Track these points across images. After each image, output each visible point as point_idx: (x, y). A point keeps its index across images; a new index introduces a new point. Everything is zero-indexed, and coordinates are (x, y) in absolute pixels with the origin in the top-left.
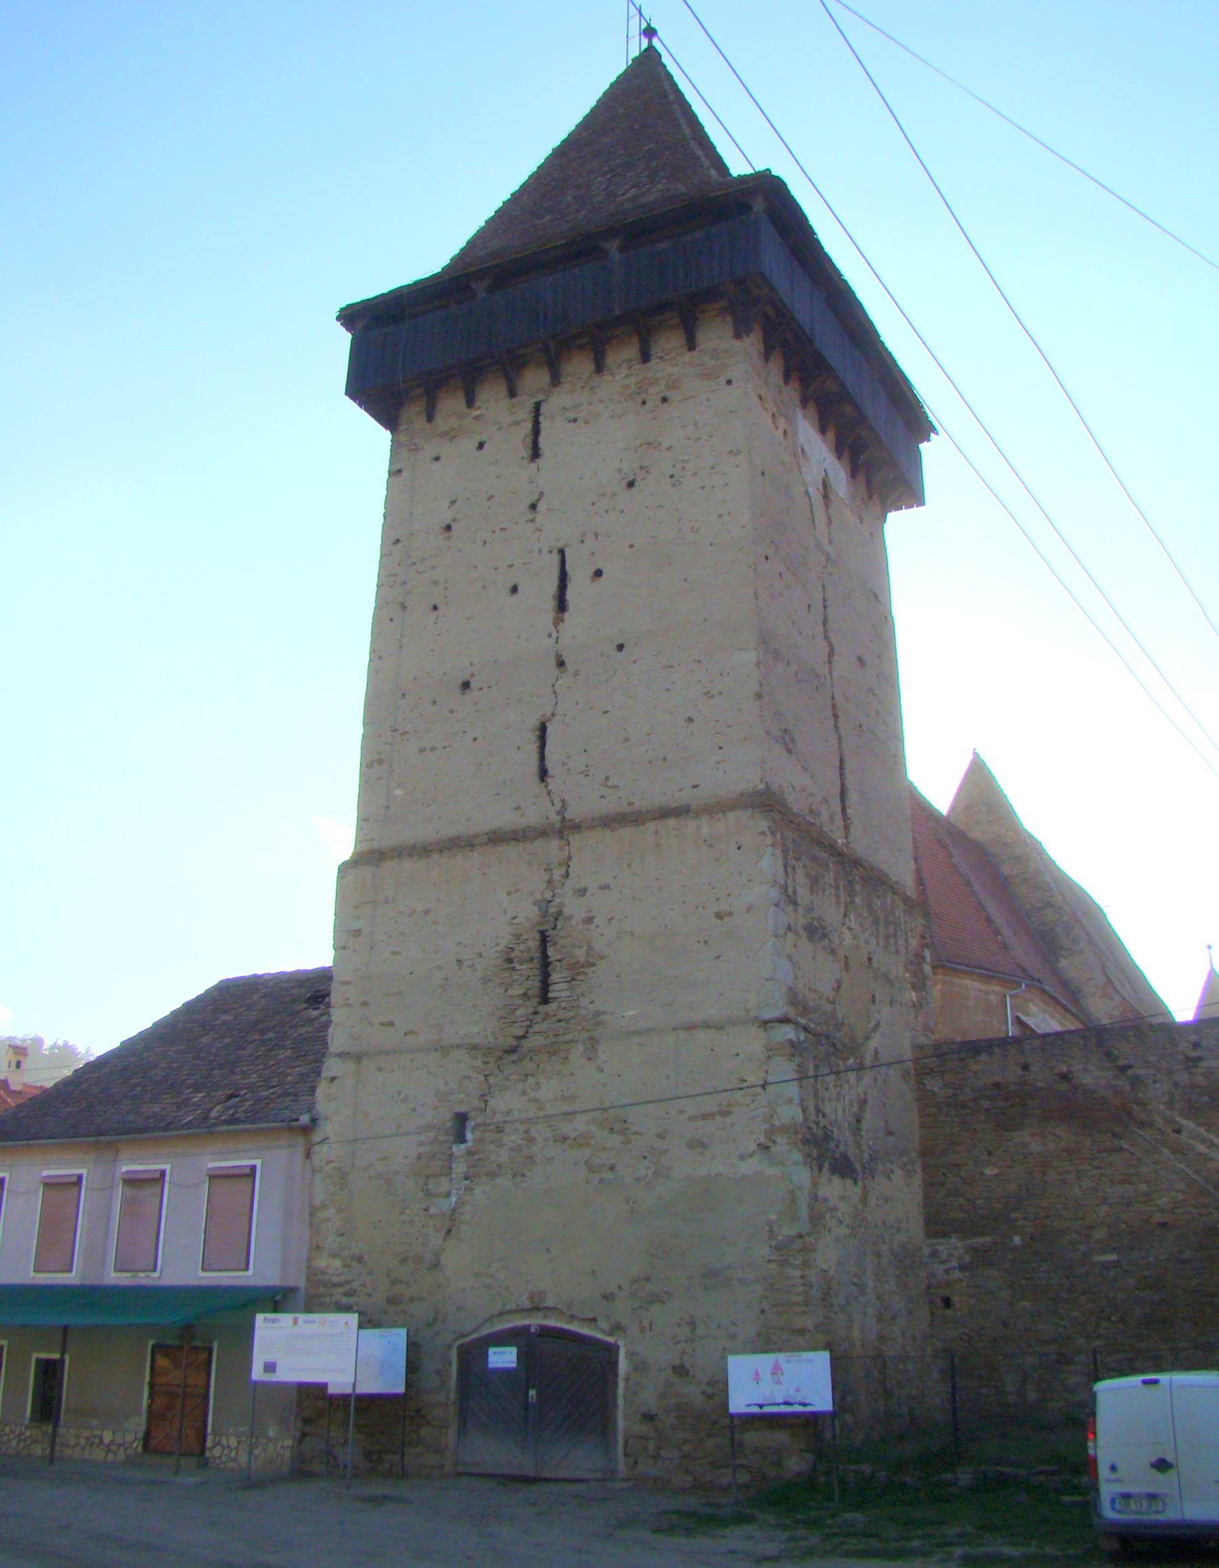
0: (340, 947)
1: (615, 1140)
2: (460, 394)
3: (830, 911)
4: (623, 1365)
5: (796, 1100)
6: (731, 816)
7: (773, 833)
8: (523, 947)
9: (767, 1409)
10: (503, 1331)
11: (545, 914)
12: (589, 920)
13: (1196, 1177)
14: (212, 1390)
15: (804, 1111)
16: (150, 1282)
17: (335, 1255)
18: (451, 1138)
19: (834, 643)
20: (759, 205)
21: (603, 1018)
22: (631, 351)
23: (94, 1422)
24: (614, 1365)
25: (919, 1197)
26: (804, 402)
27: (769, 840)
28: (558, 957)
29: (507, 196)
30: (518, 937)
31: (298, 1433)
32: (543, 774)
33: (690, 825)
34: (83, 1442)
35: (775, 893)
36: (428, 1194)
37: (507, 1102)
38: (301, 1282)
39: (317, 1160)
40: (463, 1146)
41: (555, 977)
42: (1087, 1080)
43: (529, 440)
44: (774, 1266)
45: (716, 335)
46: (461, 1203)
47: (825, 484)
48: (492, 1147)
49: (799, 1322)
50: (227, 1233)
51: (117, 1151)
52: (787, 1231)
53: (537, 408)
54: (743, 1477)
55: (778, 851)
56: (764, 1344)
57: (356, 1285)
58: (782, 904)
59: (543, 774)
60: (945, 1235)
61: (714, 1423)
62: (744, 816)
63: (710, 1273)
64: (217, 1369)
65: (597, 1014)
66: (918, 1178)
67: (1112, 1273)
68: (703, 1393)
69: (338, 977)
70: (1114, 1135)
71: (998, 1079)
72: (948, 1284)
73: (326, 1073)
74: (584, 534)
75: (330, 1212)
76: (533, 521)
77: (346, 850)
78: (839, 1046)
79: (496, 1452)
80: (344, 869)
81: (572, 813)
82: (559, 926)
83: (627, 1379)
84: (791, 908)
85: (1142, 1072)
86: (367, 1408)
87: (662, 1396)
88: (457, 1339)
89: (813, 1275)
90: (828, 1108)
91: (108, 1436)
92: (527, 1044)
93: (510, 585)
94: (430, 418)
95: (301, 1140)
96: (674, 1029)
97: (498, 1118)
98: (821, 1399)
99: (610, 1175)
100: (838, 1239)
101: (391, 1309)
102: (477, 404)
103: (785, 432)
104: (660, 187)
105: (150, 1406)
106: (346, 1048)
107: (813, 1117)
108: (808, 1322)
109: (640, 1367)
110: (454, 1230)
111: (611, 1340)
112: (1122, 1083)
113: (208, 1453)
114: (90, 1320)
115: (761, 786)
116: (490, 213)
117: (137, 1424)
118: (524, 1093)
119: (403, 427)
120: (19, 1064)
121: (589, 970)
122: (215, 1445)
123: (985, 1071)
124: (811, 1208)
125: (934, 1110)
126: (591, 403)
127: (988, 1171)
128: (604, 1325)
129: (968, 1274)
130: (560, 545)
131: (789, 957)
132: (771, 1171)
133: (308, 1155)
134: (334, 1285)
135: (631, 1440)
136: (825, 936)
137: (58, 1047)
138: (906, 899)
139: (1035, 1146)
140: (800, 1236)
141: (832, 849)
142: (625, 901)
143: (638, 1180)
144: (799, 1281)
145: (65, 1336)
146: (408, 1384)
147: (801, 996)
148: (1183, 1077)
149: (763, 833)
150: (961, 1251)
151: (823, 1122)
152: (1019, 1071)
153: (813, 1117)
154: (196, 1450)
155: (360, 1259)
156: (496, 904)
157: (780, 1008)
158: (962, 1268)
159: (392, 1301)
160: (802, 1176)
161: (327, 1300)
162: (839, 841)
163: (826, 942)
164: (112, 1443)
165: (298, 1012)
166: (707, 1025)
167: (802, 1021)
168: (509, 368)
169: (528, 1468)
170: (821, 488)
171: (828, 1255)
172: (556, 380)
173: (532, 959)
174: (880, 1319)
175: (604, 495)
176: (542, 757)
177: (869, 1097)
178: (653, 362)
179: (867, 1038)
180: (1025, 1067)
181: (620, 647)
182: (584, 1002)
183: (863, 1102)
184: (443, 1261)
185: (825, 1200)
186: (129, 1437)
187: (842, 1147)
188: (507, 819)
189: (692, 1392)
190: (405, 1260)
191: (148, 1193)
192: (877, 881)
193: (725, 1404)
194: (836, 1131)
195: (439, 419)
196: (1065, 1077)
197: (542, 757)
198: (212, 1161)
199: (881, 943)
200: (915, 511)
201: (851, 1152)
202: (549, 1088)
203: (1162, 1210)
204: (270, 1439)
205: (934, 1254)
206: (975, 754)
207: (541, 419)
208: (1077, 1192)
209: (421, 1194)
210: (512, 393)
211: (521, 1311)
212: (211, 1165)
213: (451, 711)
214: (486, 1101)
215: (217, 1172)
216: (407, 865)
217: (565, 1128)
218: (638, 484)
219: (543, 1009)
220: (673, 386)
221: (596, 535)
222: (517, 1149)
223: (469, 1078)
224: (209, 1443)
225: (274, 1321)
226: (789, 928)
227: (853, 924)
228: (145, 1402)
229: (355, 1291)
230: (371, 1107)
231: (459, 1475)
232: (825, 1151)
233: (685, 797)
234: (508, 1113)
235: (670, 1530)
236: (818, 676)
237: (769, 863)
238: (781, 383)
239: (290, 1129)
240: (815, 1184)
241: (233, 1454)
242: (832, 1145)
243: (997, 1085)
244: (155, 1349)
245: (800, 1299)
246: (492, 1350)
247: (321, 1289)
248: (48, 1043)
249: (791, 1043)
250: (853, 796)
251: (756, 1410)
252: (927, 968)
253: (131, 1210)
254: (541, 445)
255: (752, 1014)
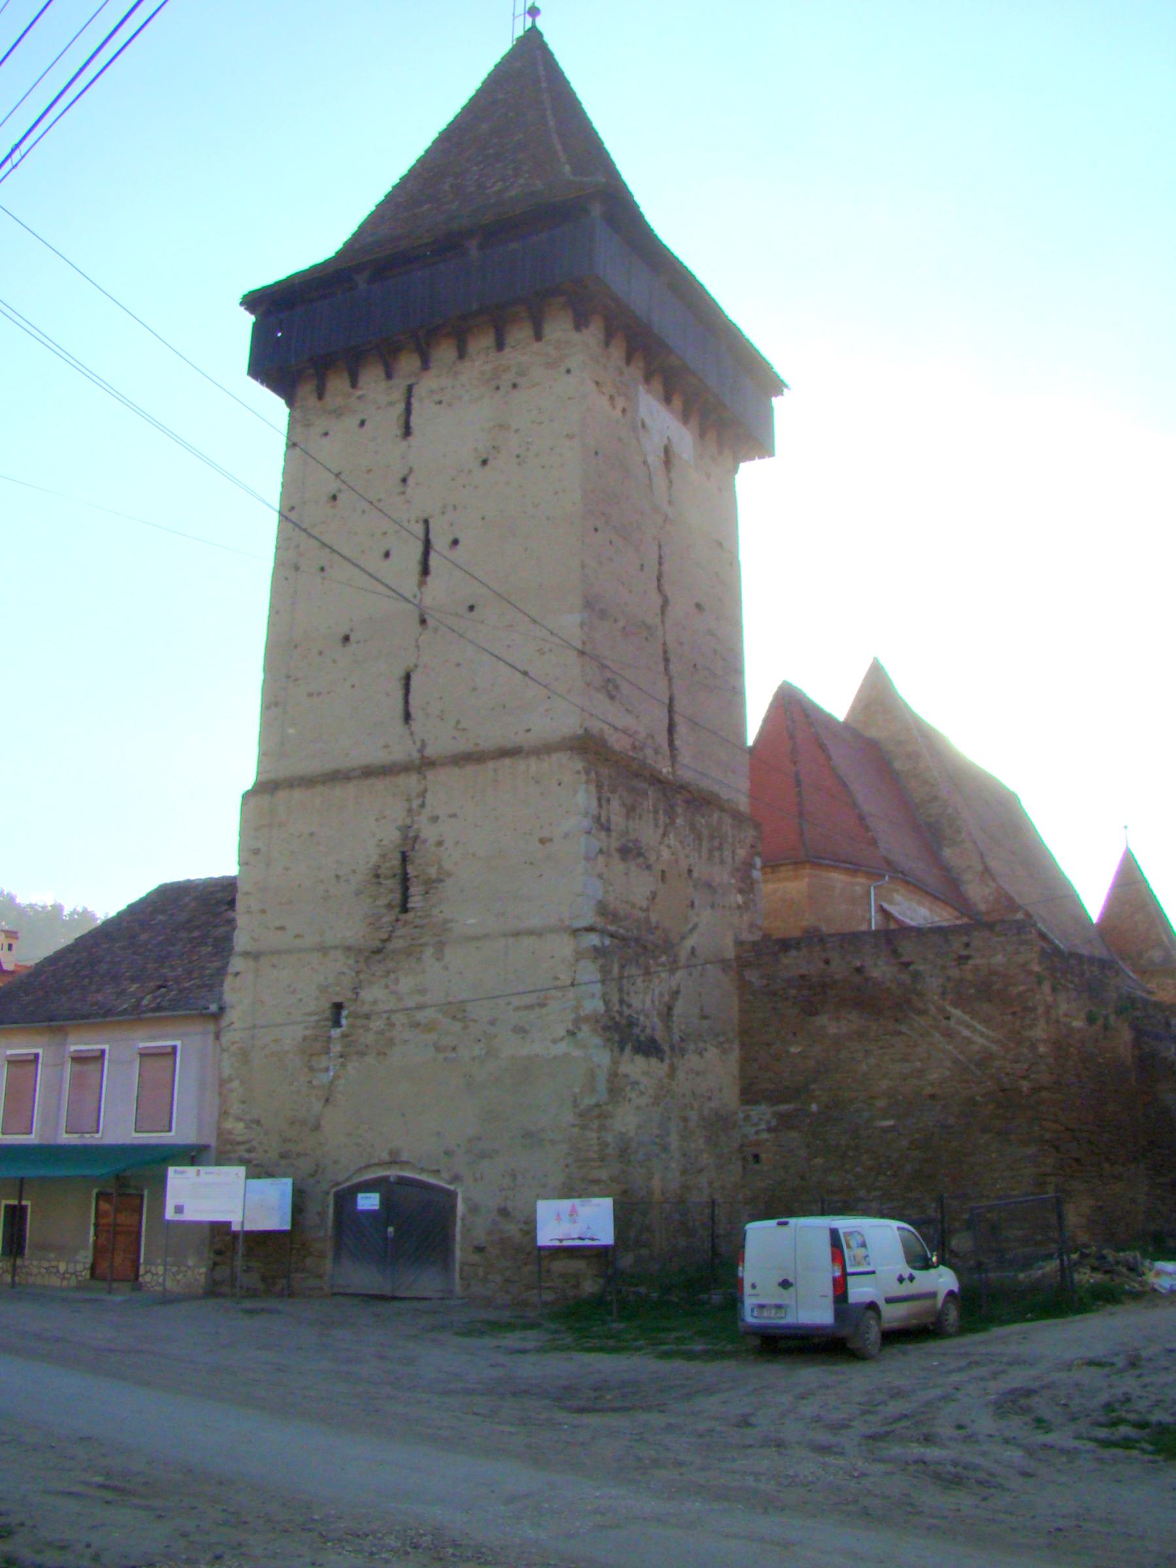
0: (243, 863)
1: (457, 1026)
2: (345, 375)
3: (647, 832)
4: (461, 1208)
5: (598, 995)
6: (555, 757)
7: (587, 773)
8: (388, 865)
9: (565, 1243)
10: (372, 1180)
11: (405, 838)
12: (440, 844)
13: (961, 1057)
14: (144, 1229)
15: (607, 1003)
16: (95, 1142)
17: (239, 1119)
18: (330, 1024)
19: (669, 594)
20: (596, 210)
21: (450, 925)
22: (486, 340)
23: (52, 1255)
24: (453, 1206)
25: (736, 1072)
26: (647, 379)
27: (583, 777)
28: (416, 873)
29: (396, 181)
30: (383, 856)
31: (211, 1263)
32: (407, 717)
33: (521, 765)
34: (43, 1271)
35: (587, 823)
36: (311, 1069)
37: (373, 994)
38: (212, 1141)
39: (225, 1039)
40: (338, 1030)
41: (412, 890)
42: (875, 974)
43: (402, 421)
44: (576, 1130)
45: (559, 328)
46: (337, 1077)
47: (667, 451)
48: (361, 1031)
49: (595, 1174)
50: (154, 1102)
51: (67, 1034)
52: (588, 1101)
53: (410, 389)
54: (548, 1296)
55: (592, 788)
56: (568, 1191)
57: (254, 1143)
58: (593, 831)
59: (407, 717)
60: (756, 1102)
61: (529, 1254)
62: (562, 757)
63: (528, 1135)
64: (148, 1208)
65: (446, 922)
66: (735, 1055)
67: (889, 1136)
68: (521, 1230)
69: (242, 887)
70: (897, 1020)
71: (804, 971)
72: (758, 1144)
73: (231, 969)
74: (445, 507)
75: (235, 1084)
76: (403, 493)
77: (248, 780)
78: (649, 946)
79: (364, 1277)
80: (247, 796)
81: (429, 752)
82: (417, 847)
83: (463, 1219)
84: (603, 834)
85: (921, 968)
86: (260, 1240)
87: (490, 1233)
88: (333, 1186)
89: (610, 1138)
90: (636, 1002)
91: (62, 1267)
92: (390, 946)
93: (383, 551)
94: (320, 396)
95: (211, 1027)
96: (504, 935)
97: (366, 1008)
98: (606, 1236)
99: (453, 1055)
100: (638, 1108)
101: (283, 1162)
102: (360, 384)
103: (624, 411)
104: (521, 181)
105: (95, 1243)
106: (249, 948)
107: (616, 1008)
108: (604, 1174)
109: (474, 1209)
110: (331, 1099)
111: (452, 1187)
112: (905, 977)
113: (141, 1279)
114: (42, 1172)
115: (580, 732)
116: (380, 198)
117: (86, 1257)
118: (387, 987)
119: (298, 405)
120: (10, 947)
121: (440, 886)
122: (146, 1272)
123: (794, 964)
124: (610, 1081)
125: (750, 997)
126: (453, 387)
127: (794, 1049)
128: (445, 1175)
129: (773, 1135)
130: (426, 516)
131: (600, 876)
132: (577, 1053)
133: (217, 1037)
134: (239, 1143)
135: (466, 1268)
136: (640, 854)
137: (78, 914)
138: (736, 815)
139: (832, 1030)
140: (598, 1105)
141: (656, 780)
142: (470, 827)
143: (473, 1059)
144: (595, 1141)
145: (22, 1186)
146: (293, 1225)
147: (611, 907)
148: (954, 973)
149: (578, 772)
150: (768, 1116)
151: (627, 1012)
152: (821, 965)
153: (616, 1008)
154: (133, 1278)
155: (258, 1122)
156: (366, 829)
157: (589, 917)
158: (769, 1130)
159: (284, 1156)
160: (603, 1058)
161: (232, 1155)
162: (664, 770)
163: (641, 860)
164: (66, 1272)
165: (220, 913)
166: (531, 932)
167: (612, 928)
168: (387, 355)
169: (387, 1290)
170: (662, 455)
171: (627, 1120)
172: (426, 365)
173: (395, 876)
174: (684, 1172)
175: (462, 471)
176: (407, 702)
177: (682, 988)
178: (507, 350)
179: (683, 938)
180: (827, 962)
181: (471, 608)
182: (436, 911)
183: (676, 994)
184: (323, 1123)
185: (626, 1076)
186: (80, 1267)
187: (648, 1031)
188: (377, 756)
189: (512, 1229)
190: (293, 1123)
191: (92, 1068)
192: (701, 801)
193: (535, 1238)
194: (642, 1018)
195: (328, 398)
196: (859, 970)
197: (407, 702)
198: (143, 1040)
199: (705, 855)
200: (771, 459)
201: (659, 1035)
202: (406, 983)
203: (932, 1084)
204: (189, 1267)
205: (747, 1118)
206: (875, 660)
207: (413, 400)
208: (865, 1068)
209: (306, 1070)
210: (389, 376)
211: (381, 1164)
212: (142, 1045)
213: (334, 661)
214: (357, 994)
215: (148, 1051)
216: (298, 794)
217: (420, 1016)
218: (491, 463)
219: (403, 917)
220: (522, 374)
221: (455, 508)
222: (381, 1032)
223: (343, 973)
224: (142, 1270)
225: (182, 1172)
226: (601, 851)
227: (672, 842)
228: (92, 1238)
229: (255, 1148)
230: (268, 997)
231: (335, 1294)
232: (624, 1033)
233: (520, 739)
234: (375, 1002)
235: (468, 1333)
236: (649, 628)
237: (583, 798)
238: (622, 364)
239: (202, 1015)
240: (615, 1063)
241: (161, 1280)
242: (636, 1030)
243: (803, 977)
244: (100, 1196)
245: (596, 1156)
246: (360, 1195)
247: (229, 1147)
248: (67, 911)
249: (595, 949)
250: (682, 729)
251: (557, 1243)
252: (756, 874)
253: (78, 1083)
254: (412, 424)
255: (567, 923)
